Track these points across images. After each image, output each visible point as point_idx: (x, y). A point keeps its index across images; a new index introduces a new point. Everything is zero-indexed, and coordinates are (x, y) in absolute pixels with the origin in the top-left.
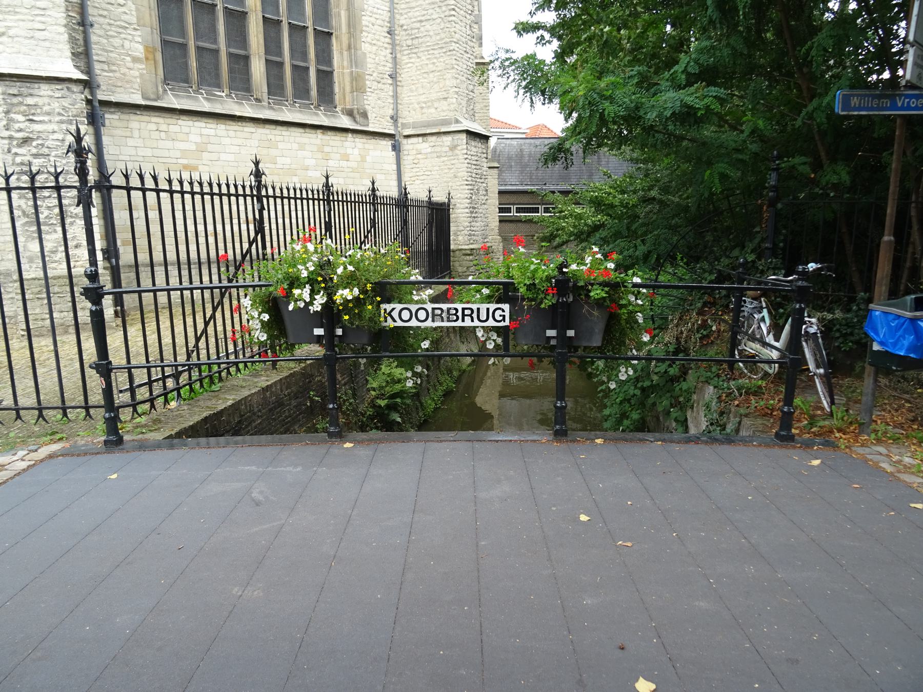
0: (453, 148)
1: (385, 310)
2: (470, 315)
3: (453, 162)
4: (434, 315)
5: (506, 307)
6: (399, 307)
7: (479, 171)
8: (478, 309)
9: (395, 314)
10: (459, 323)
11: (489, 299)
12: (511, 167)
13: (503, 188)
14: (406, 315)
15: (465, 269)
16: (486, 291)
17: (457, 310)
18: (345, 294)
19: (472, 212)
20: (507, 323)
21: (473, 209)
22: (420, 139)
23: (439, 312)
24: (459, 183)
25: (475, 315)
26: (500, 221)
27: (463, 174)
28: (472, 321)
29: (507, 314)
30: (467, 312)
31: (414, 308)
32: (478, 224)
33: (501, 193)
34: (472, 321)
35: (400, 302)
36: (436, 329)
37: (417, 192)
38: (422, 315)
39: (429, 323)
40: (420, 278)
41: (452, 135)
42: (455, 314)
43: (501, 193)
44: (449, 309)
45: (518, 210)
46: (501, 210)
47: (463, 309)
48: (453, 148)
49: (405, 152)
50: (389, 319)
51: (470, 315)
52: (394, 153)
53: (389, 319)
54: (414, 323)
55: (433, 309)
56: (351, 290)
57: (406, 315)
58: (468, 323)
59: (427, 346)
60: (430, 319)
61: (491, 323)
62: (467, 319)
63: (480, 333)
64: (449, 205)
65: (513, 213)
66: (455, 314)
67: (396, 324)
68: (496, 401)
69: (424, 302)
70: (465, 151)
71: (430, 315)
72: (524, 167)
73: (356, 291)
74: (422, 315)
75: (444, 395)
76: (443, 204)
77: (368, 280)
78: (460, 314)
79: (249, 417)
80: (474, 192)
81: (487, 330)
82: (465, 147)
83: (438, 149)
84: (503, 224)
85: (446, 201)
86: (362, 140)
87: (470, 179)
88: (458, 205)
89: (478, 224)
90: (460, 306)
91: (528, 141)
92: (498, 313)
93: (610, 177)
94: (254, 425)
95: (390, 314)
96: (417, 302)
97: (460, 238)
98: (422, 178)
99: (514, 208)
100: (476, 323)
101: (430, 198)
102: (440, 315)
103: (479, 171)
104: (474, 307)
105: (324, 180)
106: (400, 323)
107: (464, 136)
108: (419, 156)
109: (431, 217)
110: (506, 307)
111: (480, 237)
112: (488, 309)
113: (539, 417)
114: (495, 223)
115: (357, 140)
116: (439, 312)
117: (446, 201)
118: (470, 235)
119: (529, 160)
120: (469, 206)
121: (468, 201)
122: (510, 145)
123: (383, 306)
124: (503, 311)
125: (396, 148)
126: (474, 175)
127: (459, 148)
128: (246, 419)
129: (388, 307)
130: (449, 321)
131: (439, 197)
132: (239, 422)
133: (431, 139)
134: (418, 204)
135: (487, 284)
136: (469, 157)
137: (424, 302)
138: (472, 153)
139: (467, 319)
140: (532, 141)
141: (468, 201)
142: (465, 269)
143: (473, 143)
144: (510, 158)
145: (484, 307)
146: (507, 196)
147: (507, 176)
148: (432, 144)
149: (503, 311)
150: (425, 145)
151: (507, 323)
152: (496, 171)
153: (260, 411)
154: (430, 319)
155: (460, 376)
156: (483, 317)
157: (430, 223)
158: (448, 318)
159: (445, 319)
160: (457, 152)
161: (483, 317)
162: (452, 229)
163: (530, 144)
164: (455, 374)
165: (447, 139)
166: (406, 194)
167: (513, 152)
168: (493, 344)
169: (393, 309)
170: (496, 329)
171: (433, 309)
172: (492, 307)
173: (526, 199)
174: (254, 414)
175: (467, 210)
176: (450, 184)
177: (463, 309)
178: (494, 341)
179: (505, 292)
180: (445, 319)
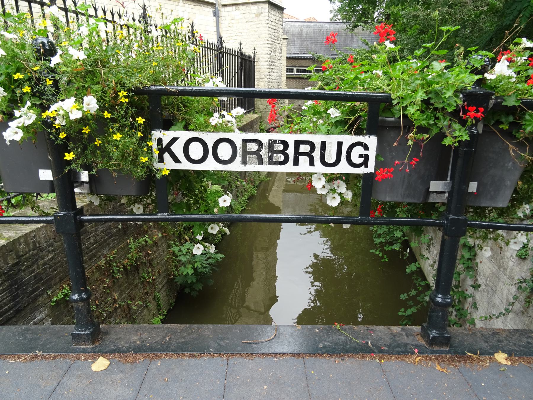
0: (258, 15)
1: (160, 141)
2: (309, 155)
3: (258, 26)
4: (245, 152)
5: (372, 141)
6: (184, 136)
7: (277, 35)
8: (323, 144)
9: (178, 149)
10: (289, 167)
11: (346, 125)
12: (294, 41)
13: (289, 55)
14: (196, 151)
15: (265, 107)
16: (335, 113)
17: (285, 144)
18: (68, 109)
19: (271, 65)
20: (371, 168)
21: (272, 63)
22: (234, 7)
23: (253, 147)
24: (262, 43)
25: (316, 155)
26: (287, 78)
27: (265, 35)
28: (312, 163)
29: (372, 153)
30: (304, 148)
31: (210, 138)
32: (275, 74)
33: (288, 58)
34: (312, 163)
35: (186, 128)
36: (243, 174)
37: (230, 44)
38: (225, 151)
39: (237, 166)
40: (222, 86)
41: (258, 5)
42: (283, 152)
43: (288, 58)
44: (272, 143)
45: (298, 71)
46: (288, 70)
47: (298, 143)
48: (258, 15)
49: (223, 18)
50: (166, 156)
51: (309, 155)
52: (214, 18)
53: (166, 156)
54: (210, 165)
55: (245, 141)
56: (79, 99)
57: (196, 151)
58: (304, 165)
59: (227, 204)
60: (239, 159)
61: (344, 168)
62: (304, 160)
63: (319, 184)
64: (254, 59)
65: (295, 73)
66: (283, 152)
67: (178, 167)
68: (281, 195)
69: (226, 129)
70: (267, 18)
71: (239, 152)
72: (302, 41)
73: (91, 104)
74: (225, 151)
75: (249, 199)
76: (249, 57)
77: (121, 84)
78: (291, 151)
79: (34, 255)
80: (272, 50)
81: (331, 178)
82: (267, 14)
83: (246, 16)
84: (288, 80)
85: (253, 55)
86: (190, 6)
87: (270, 39)
88: (261, 59)
89: (275, 74)
90: (291, 139)
91: (306, 24)
92: (358, 151)
93: (367, 44)
94: (41, 262)
95: (168, 149)
96: (216, 129)
97: (262, 84)
98: (235, 38)
99: (295, 69)
100: (319, 168)
101: (240, 50)
102: (257, 153)
103: (277, 35)
104: (317, 139)
105: (142, 11)
106: (185, 165)
107: (266, 6)
108: (233, 21)
109: (241, 64)
110: (372, 141)
111: (276, 84)
112: (340, 145)
113: (310, 208)
114: (284, 78)
115: (186, 5)
116: (253, 147)
117: (253, 55)
118: (269, 82)
119: (306, 37)
120: (269, 60)
121: (269, 56)
122: (294, 26)
123: (157, 134)
124: (366, 148)
125: (216, 14)
126: (273, 37)
127: (263, 15)
128: (27, 260)
129: (166, 136)
130: (271, 162)
131: (248, 51)
132: (17, 264)
133: (241, 7)
134: (231, 53)
135: (337, 99)
136: (270, 23)
137: (226, 129)
138: (272, 20)
139: (304, 160)
140: (309, 24)
141: (269, 56)
142: (265, 107)
143: (273, 12)
144: (293, 35)
145: (332, 141)
146: (291, 61)
147: (292, 47)
148: (243, 12)
149: (366, 148)
150: (238, 12)
151: (371, 168)
152: (285, 41)
153: (51, 245)
154: (239, 159)
155: (260, 183)
156: (331, 157)
157: (240, 70)
158: (270, 158)
159: (265, 159)
160: (260, 18)
161: (331, 157)
162: (256, 77)
163: (307, 26)
164: (257, 182)
165: (254, 8)
166: (221, 42)
167: (296, 31)
168: (338, 200)
169: (174, 140)
170: (347, 178)
171: (245, 141)
172: (348, 140)
173: (303, 63)
174: (42, 250)
175: (267, 63)
176: (255, 43)
177: (298, 143)
178: (340, 194)
179: (374, 115)
180: (265, 159)
